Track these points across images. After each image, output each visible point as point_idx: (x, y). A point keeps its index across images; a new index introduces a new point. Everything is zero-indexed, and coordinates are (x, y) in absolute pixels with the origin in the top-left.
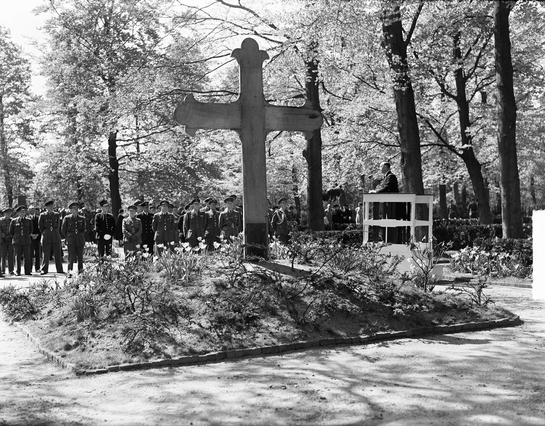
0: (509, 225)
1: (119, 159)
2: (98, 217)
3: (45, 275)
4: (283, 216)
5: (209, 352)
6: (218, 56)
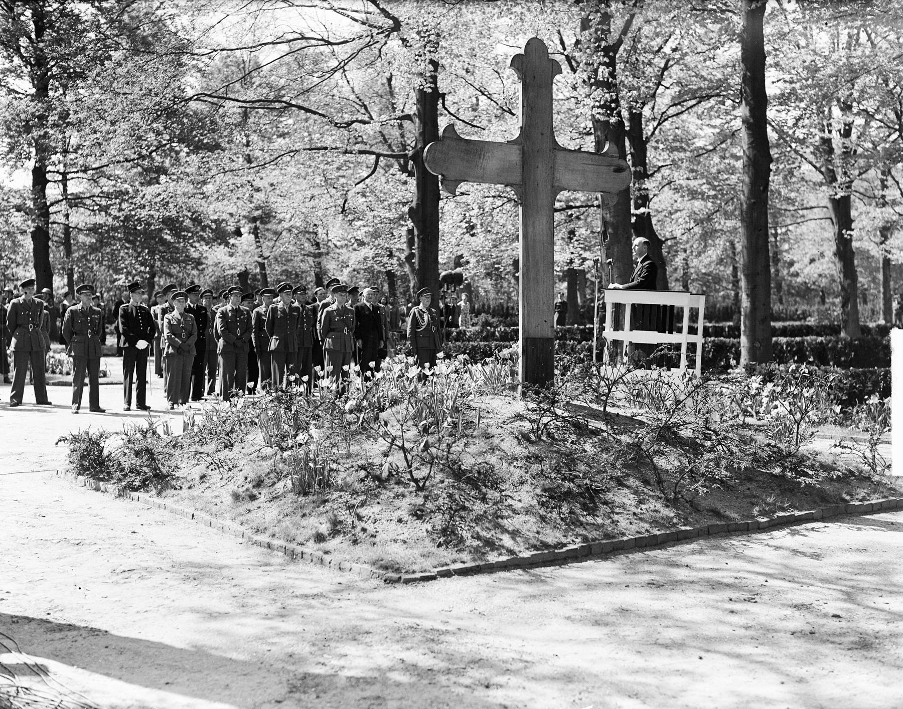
0: (752, 339)
1: (52, 204)
2: (124, 310)
3: (19, 407)
4: (426, 317)
5: (565, 545)
6: (278, 41)
